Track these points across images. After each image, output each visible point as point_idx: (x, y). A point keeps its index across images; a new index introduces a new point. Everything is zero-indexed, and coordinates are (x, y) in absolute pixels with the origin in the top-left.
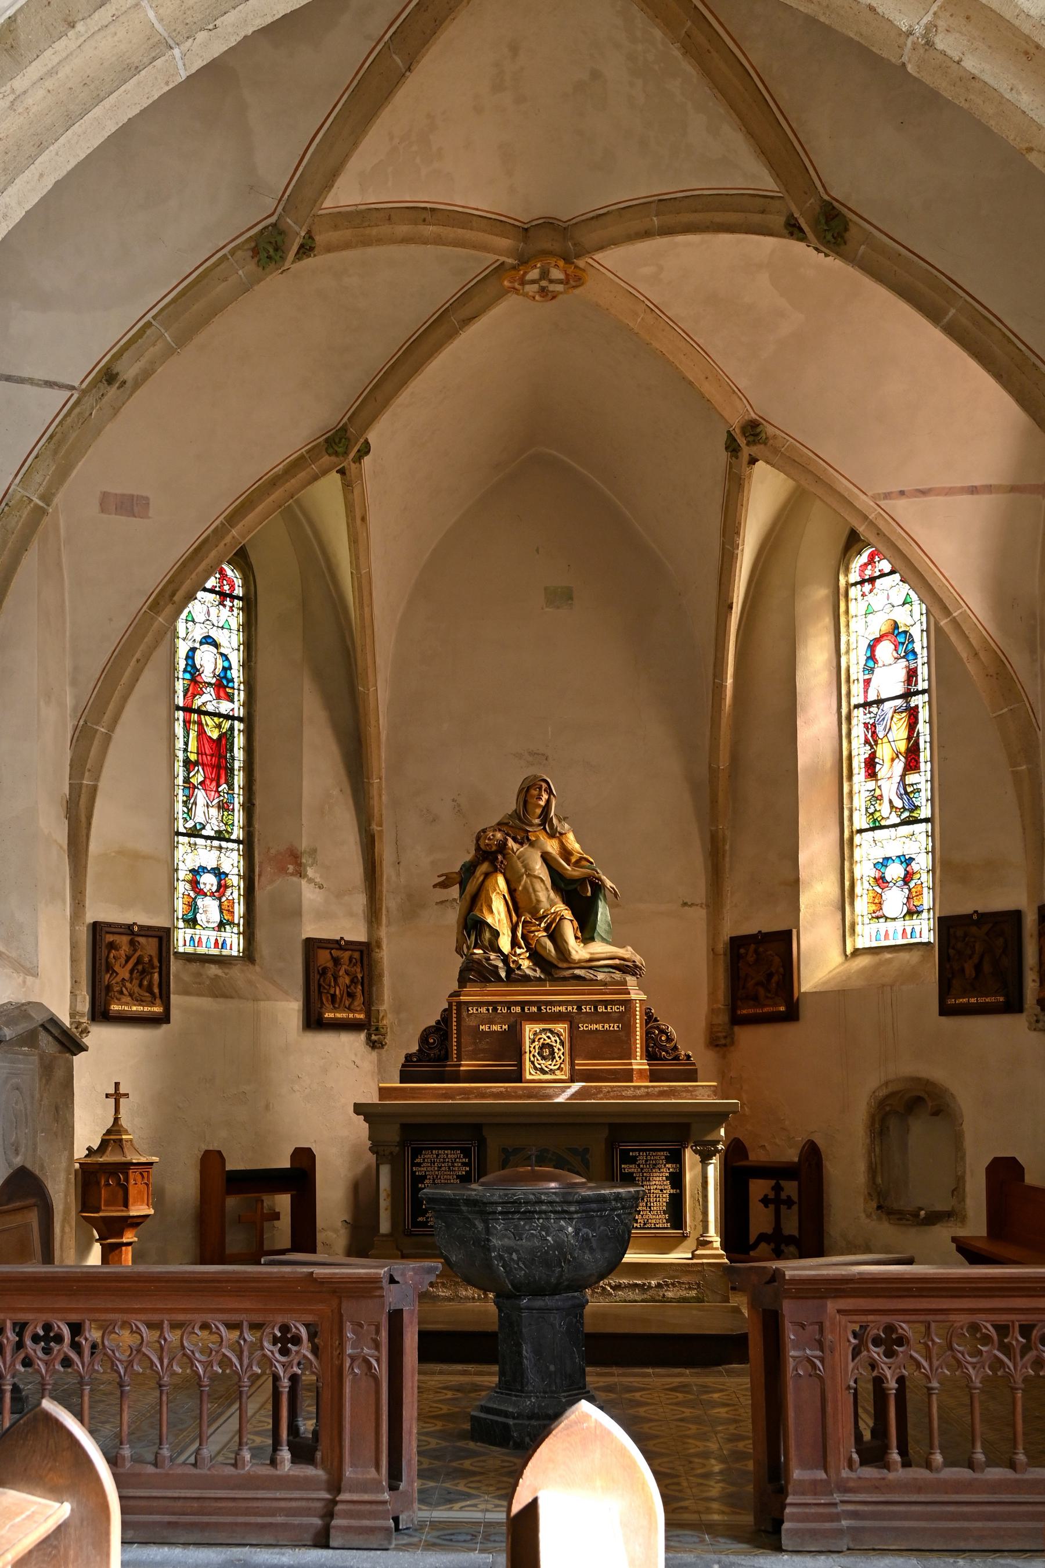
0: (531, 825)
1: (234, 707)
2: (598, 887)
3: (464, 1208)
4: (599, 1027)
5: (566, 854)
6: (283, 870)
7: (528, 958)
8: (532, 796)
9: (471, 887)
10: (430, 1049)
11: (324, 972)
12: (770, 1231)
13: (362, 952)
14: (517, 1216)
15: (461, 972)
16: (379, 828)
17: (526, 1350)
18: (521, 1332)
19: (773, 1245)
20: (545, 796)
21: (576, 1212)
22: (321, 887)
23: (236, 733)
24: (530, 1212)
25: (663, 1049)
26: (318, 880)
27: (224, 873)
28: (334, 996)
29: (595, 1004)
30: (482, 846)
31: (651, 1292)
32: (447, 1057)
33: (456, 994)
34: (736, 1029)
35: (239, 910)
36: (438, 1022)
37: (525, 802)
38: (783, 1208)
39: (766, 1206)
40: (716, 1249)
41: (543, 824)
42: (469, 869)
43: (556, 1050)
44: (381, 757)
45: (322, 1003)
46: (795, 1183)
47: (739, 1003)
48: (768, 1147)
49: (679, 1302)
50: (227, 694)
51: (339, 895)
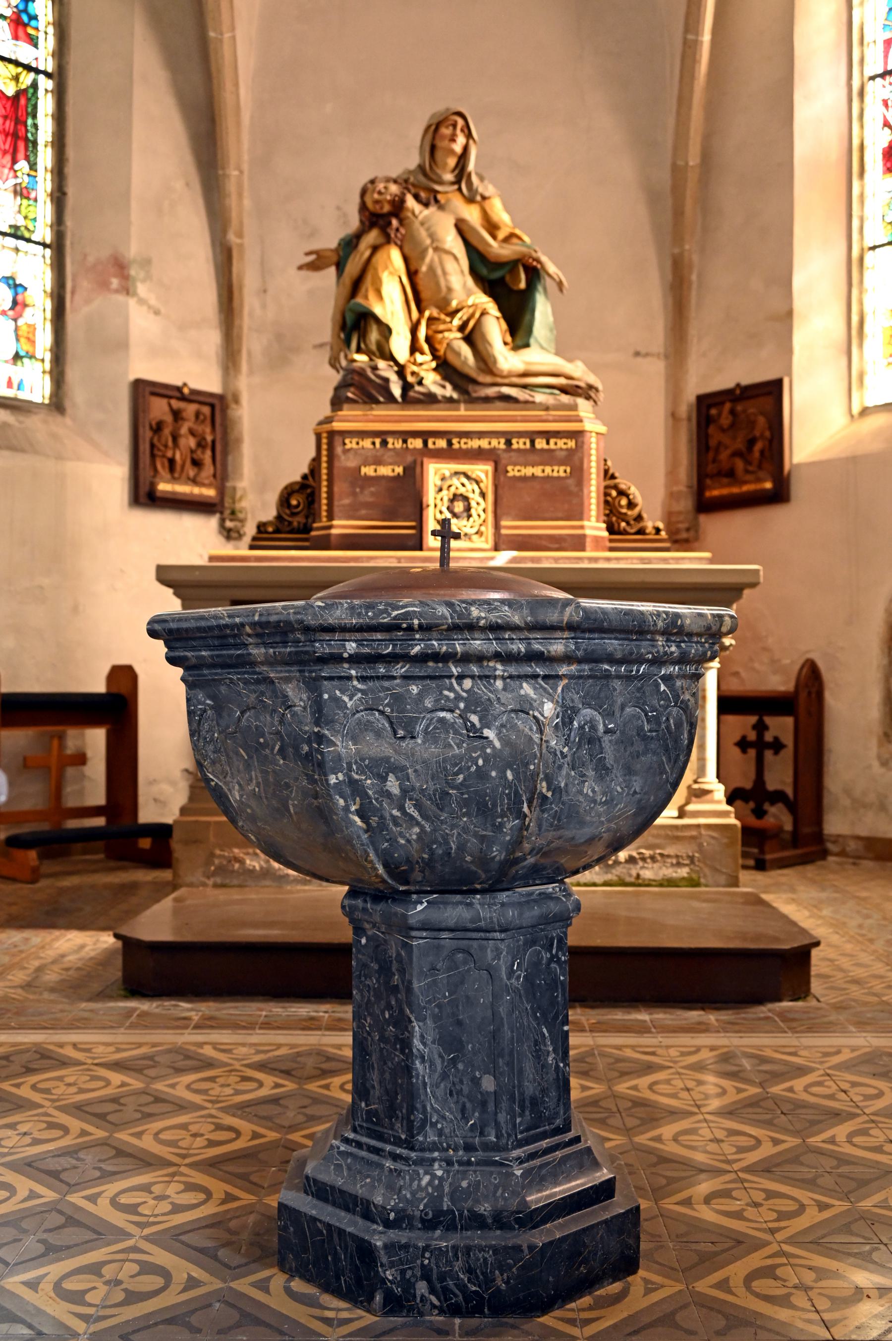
0: (441, 182)
1: (43, 55)
2: (534, 273)
3: (257, 652)
4: (537, 471)
5: (492, 227)
6: (104, 285)
7: (435, 370)
8: (443, 137)
9: (353, 267)
10: (293, 514)
11: (158, 428)
12: (748, 785)
13: (212, 406)
14: (401, 669)
15: (336, 389)
16: (238, 241)
17: (422, 1037)
18: (409, 989)
19: (752, 805)
20: (461, 140)
21: (567, 659)
22: (157, 313)
23: (41, 93)
24: (437, 657)
25: (623, 517)
26: (153, 301)
27: (21, 285)
28: (172, 462)
29: (532, 436)
30: (370, 205)
31: (619, 871)
32: (316, 516)
33: (328, 420)
34: (703, 519)
35: (45, 339)
36: (305, 477)
37: (433, 148)
38: (768, 754)
39: (744, 751)
40: (719, 802)
41: (458, 181)
42: (350, 244)
43: (473, 504)
44: (241, 143)
45: (156, 470)
46: (789, 721)
47: (708, 482)
48: (743, 674)
49: (661, 885)
50: (28, 35)
51: (183, 327)
